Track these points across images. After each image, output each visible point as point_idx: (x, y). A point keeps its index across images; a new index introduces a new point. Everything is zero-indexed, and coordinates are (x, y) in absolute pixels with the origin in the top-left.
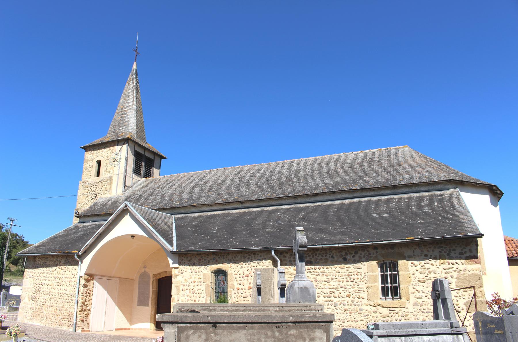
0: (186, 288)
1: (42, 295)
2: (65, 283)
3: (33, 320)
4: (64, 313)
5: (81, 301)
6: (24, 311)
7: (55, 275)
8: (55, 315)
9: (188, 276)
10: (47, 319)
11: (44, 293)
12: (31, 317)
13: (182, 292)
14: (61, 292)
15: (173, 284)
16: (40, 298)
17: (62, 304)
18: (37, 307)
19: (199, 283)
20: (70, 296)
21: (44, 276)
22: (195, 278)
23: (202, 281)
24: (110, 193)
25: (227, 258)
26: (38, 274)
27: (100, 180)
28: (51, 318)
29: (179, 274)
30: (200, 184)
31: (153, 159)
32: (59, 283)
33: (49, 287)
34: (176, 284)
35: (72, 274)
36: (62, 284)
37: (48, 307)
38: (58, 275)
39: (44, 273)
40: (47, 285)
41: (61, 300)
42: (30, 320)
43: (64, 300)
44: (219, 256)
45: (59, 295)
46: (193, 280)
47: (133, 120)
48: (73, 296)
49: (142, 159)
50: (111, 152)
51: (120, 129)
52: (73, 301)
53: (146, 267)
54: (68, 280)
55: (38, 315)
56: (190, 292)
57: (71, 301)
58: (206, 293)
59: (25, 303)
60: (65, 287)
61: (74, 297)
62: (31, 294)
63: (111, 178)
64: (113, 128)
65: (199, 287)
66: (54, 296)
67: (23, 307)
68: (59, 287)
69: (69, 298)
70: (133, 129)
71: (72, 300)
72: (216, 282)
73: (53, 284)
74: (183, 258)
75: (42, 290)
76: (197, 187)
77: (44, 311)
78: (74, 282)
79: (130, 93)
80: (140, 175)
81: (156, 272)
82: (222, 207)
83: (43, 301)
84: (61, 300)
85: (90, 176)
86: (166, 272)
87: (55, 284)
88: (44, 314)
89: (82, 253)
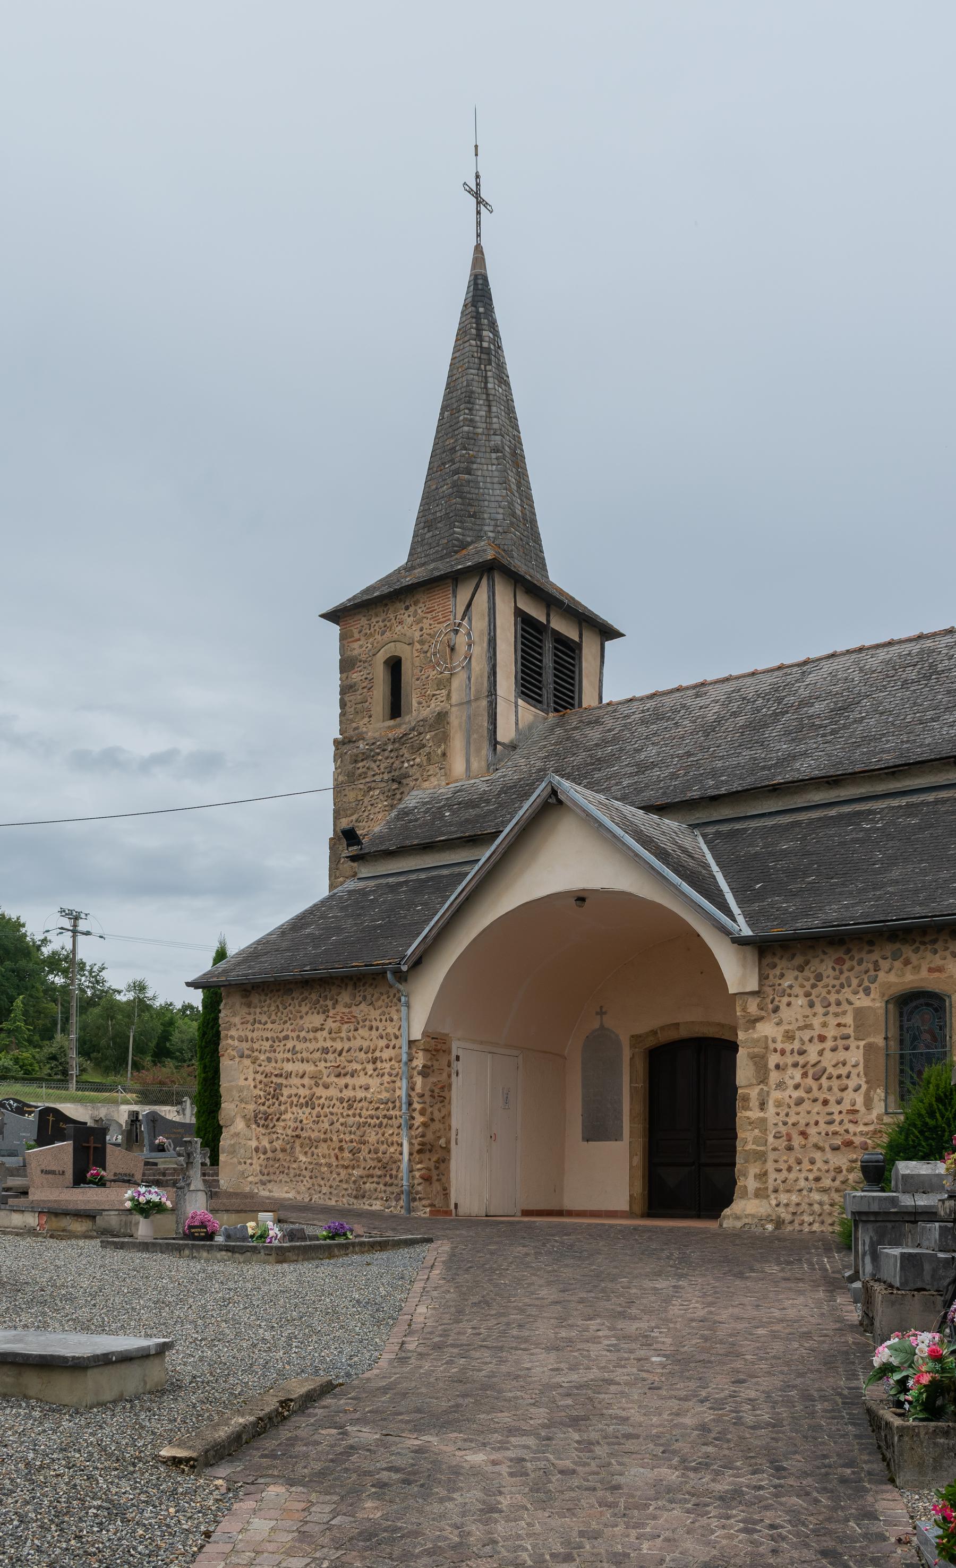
0: (789, 1060)
1: (287, 1108)
2: (359, 1067)
3: (269, 1186)
4: (367, 1158)
5: (419, 1119)
6: (235, 1160)
7: (321, 1044)
8: (337, 1166)
9: (797, 1020)
10: (314, 1180)
11: (295, 1103)
12: (260, 1177)
13: (774, 1076)
14: (348, 1093)
15: (740, 1049)
16: (283, 1117)
17: (358, 1133)
18: (277, 1144)
19: (840, 1043)
20: (382, 1106)
21: (287, 1048)
22: (824, 1025)
23: (852, 1034)
24: (446, 774)
25: (946, 949)
26: (265, 1043)
27: (399, 732)
28: (325, 1176)
29: (763, 1013)
30: (775, 714)
31: (577, 639)
32: (338, 1067)
33: (306, 1081)
34: (751, 1050)
35: (382, 1038)
36: (349, 1069)
37: (313, 1143)
38: (334, 1044)
39: (286, 1038)
40: (300, 1074)
41: (351, 1120)
42: (259, 1185)
43: (363, 1120)
44: (917, 944)
45: (345, 1104)
46: (815, 1034)
47: (498, 492)
48: (390, 1105)
49: (540, 641)
50: (431, 622)
51: (455, 533)
52: (395, 1122)
53: (605, 1013)
54: (370, 1055)
55: (281, 1169)
56: (805, 1075)
57: (385, 1121)
58: (866, 1075)
59: (237, 1135)
60: (362, 1080)
61: (394, 1108)
62: (252, 1107)
63: (442, 717)
64: (429, 531)
65: (841, 1055)
66: (328, 1111)
67: (233, 1146)
68: (342, 1081)
69: (379, 1113)
70: (499, 528)
71: (391, 1118)
72: (901, 1035)
73: (320, 1071)
74: (776, 960)
75: (286, 1092)
76: (766, 726)
77: (302, 1158)
78: (391, 1060)
79: (473, 380)
80: (540, 702)
81: (642, 1028)
82: (881, 788)
83: (293, 1125)
84: (351, 1120)
85: (366, 719)
86: (677, 1025)
87: (325, 1072)
88: (302, 1164)
89: (410, 963)
